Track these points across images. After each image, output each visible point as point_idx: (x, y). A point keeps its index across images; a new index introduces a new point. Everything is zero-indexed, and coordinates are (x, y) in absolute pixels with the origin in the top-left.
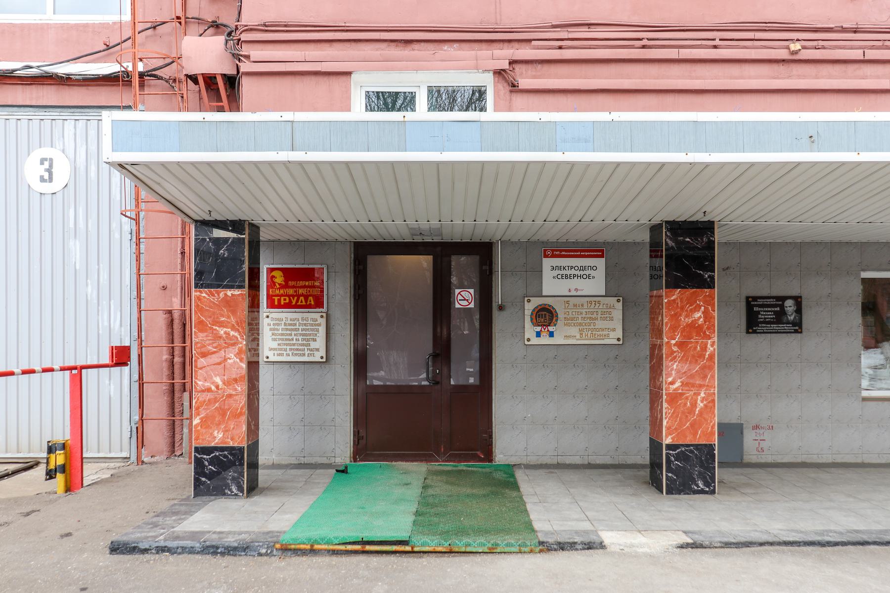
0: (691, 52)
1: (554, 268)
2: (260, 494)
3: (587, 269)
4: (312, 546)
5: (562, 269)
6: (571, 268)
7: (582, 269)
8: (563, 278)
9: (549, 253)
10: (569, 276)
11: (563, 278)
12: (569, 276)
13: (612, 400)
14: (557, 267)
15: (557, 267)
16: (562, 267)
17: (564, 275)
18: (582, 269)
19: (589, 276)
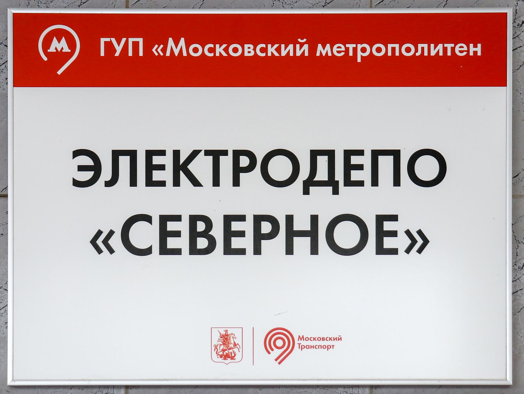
0: (420, 11)
1: (97, 168)
2: (120, 388)
3: (365, 175)
4: (226, 331)
5: (167, 175)
6: (237, 170)
7: (322, 175)
8: (172, 243)
9: (62, 45)
10: (218, 232)
11: (172, 243)
12: (218, 232)
13: (49, 4)
14: (124, 162)
15: (124, 162)
16: (168, 160)
17: (183, 227)
18: (322, 175)
19: (381, 234)
